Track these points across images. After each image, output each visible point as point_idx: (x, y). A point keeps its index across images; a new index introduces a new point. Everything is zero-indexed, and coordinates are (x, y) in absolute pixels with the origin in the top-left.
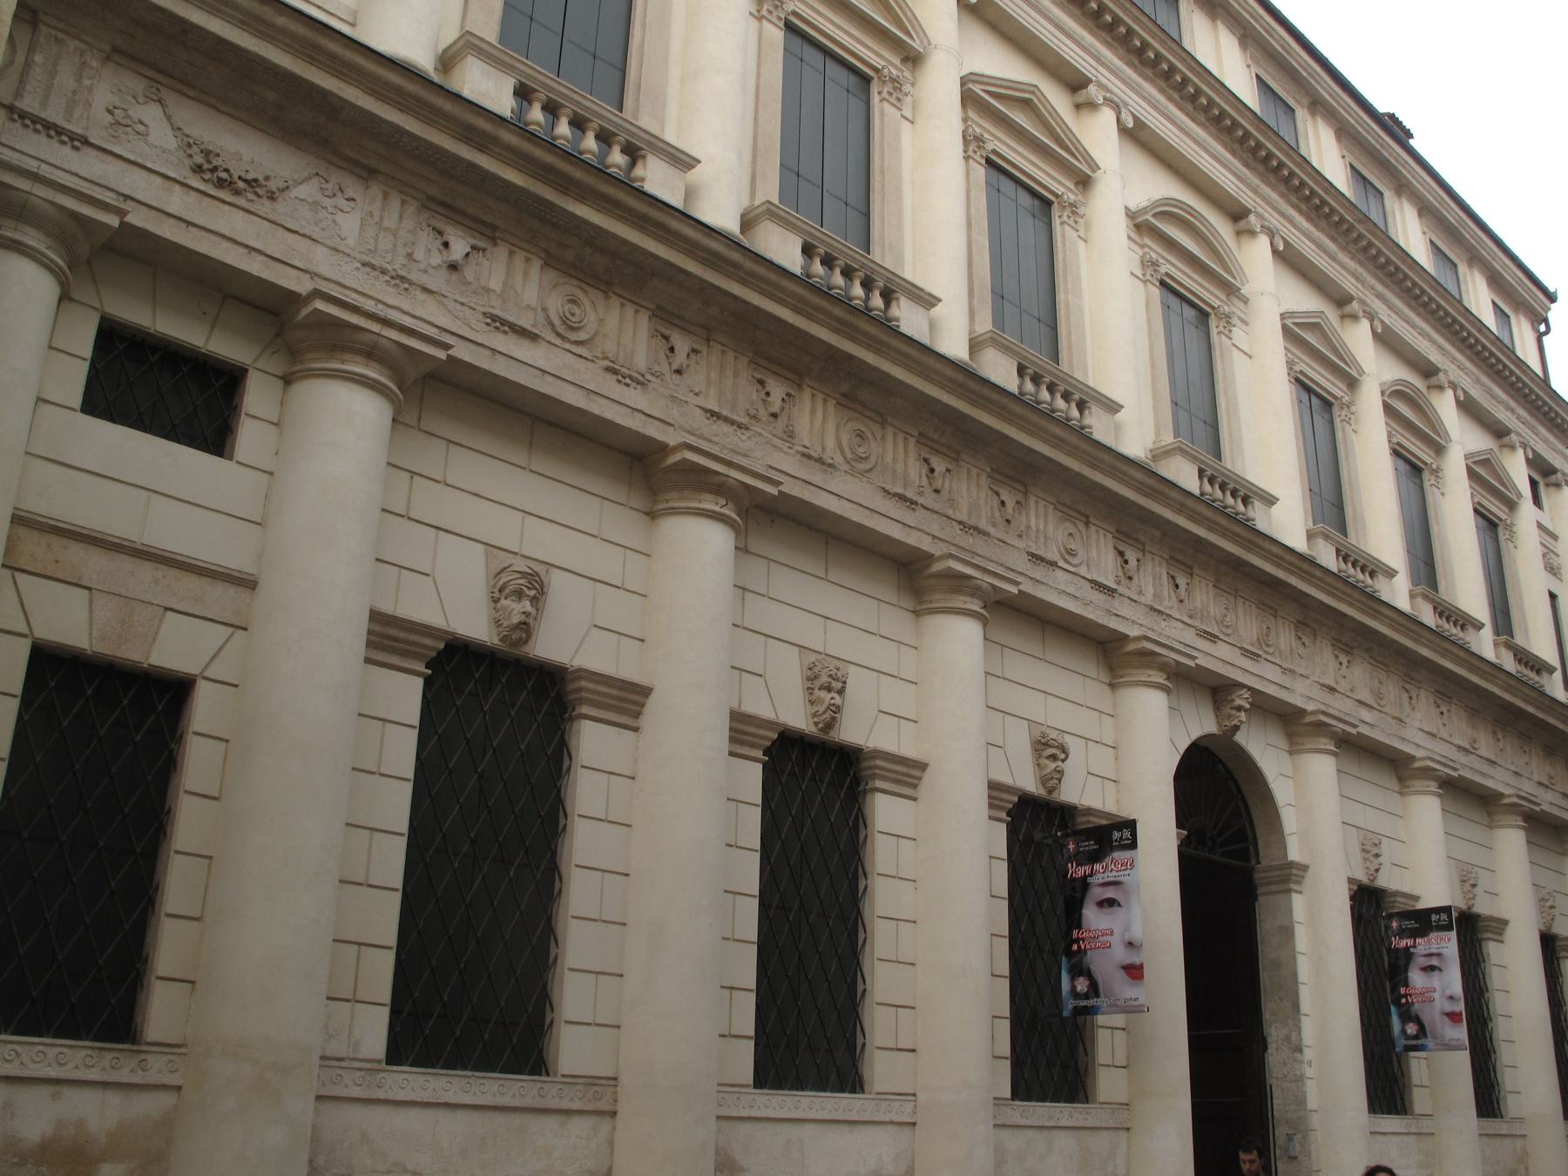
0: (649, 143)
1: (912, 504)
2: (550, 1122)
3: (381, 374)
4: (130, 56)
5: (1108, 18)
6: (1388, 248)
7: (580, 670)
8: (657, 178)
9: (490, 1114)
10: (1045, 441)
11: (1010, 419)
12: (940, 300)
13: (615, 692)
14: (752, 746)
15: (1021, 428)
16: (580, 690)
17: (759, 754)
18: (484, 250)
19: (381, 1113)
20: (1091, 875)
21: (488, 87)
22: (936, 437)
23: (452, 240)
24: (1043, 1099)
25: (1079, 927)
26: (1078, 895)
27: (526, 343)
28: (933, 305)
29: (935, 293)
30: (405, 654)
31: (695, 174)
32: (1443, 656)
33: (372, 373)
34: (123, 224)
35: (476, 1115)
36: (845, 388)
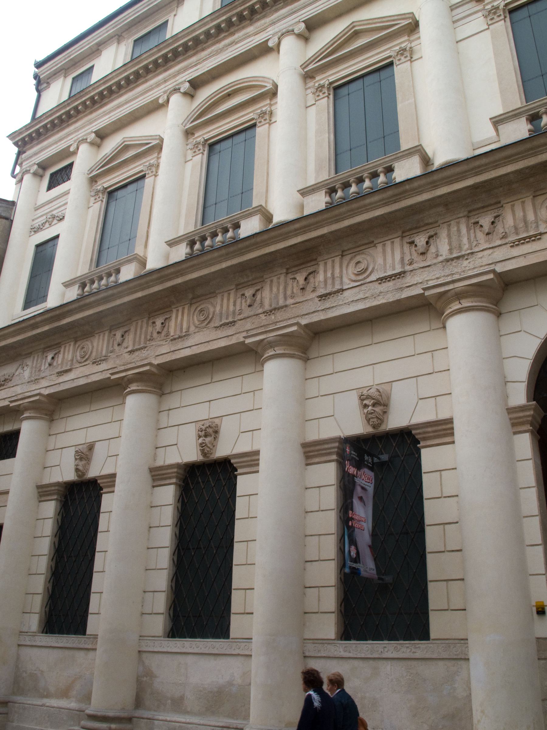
1: (233, 323)
2: (82, 653)
3: (480, 302)
4: (49, 347)
5: (234, 19)
6: (81, 97)
9: (64, 650)
10: (296, 235)
11: (266, 244)
13: (109, 480)
14: (170, 478)
15: (361, 213)
17: (334, 457)
18: (436, 234)
19: (36, 650)
22: (246, 280)
23: (28, 363)
24: (68, 633)
27: (69, 373)
32: (242, 254)
33: (466, 303)
35: (60, 650)
36: (190, 296)
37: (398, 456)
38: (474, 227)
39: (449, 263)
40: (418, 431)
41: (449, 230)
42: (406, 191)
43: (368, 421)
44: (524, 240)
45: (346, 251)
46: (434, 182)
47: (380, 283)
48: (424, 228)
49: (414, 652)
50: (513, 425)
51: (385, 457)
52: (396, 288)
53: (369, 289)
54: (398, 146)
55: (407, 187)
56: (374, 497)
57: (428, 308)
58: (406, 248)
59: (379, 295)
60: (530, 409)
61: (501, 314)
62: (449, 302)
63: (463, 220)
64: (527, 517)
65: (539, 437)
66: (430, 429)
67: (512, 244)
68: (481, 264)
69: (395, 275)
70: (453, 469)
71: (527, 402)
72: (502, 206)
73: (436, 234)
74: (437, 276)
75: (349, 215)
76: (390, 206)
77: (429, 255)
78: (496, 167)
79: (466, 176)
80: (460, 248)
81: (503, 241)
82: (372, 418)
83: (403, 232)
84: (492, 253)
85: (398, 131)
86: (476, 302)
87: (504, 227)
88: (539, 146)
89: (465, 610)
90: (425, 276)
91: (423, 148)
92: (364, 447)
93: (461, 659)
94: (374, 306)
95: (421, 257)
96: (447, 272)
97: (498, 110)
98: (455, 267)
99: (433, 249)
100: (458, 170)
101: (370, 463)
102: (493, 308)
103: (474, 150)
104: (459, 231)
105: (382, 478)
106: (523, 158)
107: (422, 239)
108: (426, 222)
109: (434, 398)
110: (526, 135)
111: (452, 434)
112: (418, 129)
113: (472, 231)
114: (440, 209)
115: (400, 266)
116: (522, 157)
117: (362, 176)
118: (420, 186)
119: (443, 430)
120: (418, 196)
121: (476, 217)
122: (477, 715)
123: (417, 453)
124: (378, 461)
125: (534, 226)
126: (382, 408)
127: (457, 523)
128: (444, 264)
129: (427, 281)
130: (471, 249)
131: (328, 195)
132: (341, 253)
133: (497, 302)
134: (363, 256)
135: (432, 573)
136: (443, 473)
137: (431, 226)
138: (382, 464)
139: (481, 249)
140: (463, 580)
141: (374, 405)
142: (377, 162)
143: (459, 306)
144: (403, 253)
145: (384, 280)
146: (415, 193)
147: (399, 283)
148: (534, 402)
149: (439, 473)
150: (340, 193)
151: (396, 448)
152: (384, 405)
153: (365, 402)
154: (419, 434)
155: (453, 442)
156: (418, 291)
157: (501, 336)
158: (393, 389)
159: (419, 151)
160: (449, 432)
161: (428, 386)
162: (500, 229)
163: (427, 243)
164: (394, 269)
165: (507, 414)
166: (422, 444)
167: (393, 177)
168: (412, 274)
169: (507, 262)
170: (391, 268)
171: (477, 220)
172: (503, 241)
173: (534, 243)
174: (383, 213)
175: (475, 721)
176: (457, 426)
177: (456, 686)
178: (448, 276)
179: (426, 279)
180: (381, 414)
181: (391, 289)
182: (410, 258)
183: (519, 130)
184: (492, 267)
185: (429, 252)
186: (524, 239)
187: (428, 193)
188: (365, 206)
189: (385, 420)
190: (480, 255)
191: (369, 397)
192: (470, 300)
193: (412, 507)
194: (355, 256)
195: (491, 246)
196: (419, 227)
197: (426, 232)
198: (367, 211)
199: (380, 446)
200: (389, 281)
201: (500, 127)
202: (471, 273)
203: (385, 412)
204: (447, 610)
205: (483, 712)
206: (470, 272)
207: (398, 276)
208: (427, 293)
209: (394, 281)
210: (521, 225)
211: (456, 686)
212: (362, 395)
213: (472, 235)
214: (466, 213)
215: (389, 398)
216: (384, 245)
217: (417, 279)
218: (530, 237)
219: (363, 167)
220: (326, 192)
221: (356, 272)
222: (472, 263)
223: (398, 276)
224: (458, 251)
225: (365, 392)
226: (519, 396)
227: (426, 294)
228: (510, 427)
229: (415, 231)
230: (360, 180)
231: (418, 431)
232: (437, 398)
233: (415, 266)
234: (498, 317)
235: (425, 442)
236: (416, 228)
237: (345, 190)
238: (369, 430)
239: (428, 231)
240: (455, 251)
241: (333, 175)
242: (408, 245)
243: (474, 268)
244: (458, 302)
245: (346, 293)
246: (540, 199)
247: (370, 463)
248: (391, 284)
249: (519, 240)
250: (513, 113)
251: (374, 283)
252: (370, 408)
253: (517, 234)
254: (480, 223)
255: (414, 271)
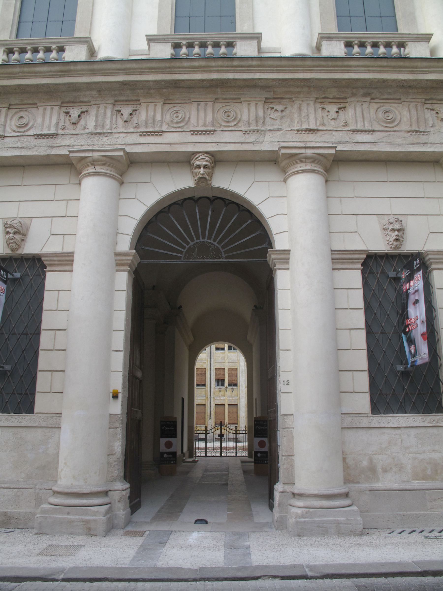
0: (236, 38)
7: (427, 251)
8: (415, 50)
12: (432, 34)
14: (357, 263)
15: (31, 77)
16: (429, 259)
17: (359, 266)
18: (87, 111)
20: (409, 289)
21: (336, 49)
25: (408, 318)
26: (405, 302)
28: (429, 39)
29: (428, 32)
30: (353, 263)
31: (433, 40)
33: (99, 169)
34: (336, 151)
37: (29, 276)
38: (117, 114)
39: (92, 136)
40: (46, 259)
41: (98, 111)
42: (70, 71)
43: (8, 244)
44: (150, 133)
45: (13, 105)
46: (94, 70)
47: (36, 138)
48: (79, 104)
49: (21, 422)
50: (117, 265)
51: (17, 275)
52: (48, 145)
53: (26, 141)
54: (73, 33)
55: (72, 68)
56: (5, 304)
57: (70, 166)
58: (62, 116)
59: (33, 148)
60: (130, 255)
61: (123, 183)
62: (87, 166)
63: (110, 106)
64: (116, 331)
65: (134, 276)
66: (55, 259)
67: (141, 134)
68: (116, 143)
69: (49, 135)
70: (68, 290)
71: (130, 250)
72: (140, 104)
73: (87, 111)
74: (82, 144)
75: (20, 76)
76: (56, 79)
77: (79, 126)
78: (142, 73)
79: (118, 73)
80: (103, 127)
81: (135, 130)
82: (12, 243)
83: (62, 103)
84: (125, 137)
85: (75, 20)
86: (107, 170)
87: (138, 120)
88: (175, 68)
89: (62, 393)
90: (73, 141)
91: (91, 40)
92: (2, 265)
93: (55, 427)
94: (28, 156)
95: (73, 126)
96: (90, 142)
97: (154, 31)
98: (97, 140)
99: (82, 122)
100: (113, 66)
101: (4, 277)
102: (118, 177)
103: (130, 55)
104: (105, 113)
105: (13, 290)
106: (163, 73)
107: (76, 112)
108: (82, 100)
109: (63, 236)
110: (169, 57)
111: (72, 265)
112: (91, 25)
113: (115, 116)
114: (94, 93)
115: (55, 129)
116: (162, 72)
117: (38, 47)
118: (83, 70)
119: (65, 260)
120: (79, 77)
121: (120, 106)
122: (61, 465)
123: (43, 275)
124: (12, 277)
125: (159, 124)
126: (21, 236)
127: (65, 330)
128: (89, 136)
129: (74, 145)
130: (111, 130)
131: (5, 54)
132: (8, 106)
133: (122, 174)
134: (26, 113)
135: (42, 364)
136: (60, 292)
137: (85, 104)
138: (15, 280)
139: (119, 132)
140: (64, 371)
141: (15, 233)
142: (53, 40)
143: (94, 170)
144: (59, 119)
145: (40, 137)
146: (77, 74)
147: (51, 142)
148: (135, 251)
149: (57, 292)
150: (16, 56)
151: (28, 269)
152: (23, 235)
153: (8, 230)
154: (47, 261)
155: (71, 271)
156: (64, 151)
157: (120, 199)
158: (32, 224)
159: (87, 41)
160: (69, 262)
161: (61, 226)
162: (135, 120)
163: (79, 116)
164: (49, 130)
165: (114, 256)
166: (48, 268)
167: (63, 56)
168: (63, 137)
169: (135, 146)
170: (47, 129)
171: (120, 109)
172: (135, 130)
173: (157, 137)
174: (48, 82)
175: (59, 470)
176: (77, 259)
177: (49, 446)
178: (90, 145)
179: (73, 144)
180: (20, 241)
181: (44, 145)
182: (63, 124)
183: (164, 51)
184: (123, 147)
185: (79, 123)
186: (150, 132)
187: (88, 78)
188: (35, 72)
189: (22, 246)
190: (117, 135)
191: (11, 226)
192: (102, 167)
193: (33, 315)
194: (20, 111)
195: (126, 131)
196: (76, 102)
197: (80, 107)
198: (36, 77)
199: (15, 266)
200: (43, 138)
201: (152, 45)
202: (107, 148)
203: (23, 240)
204: (49, 392)
205: (65, 464)
206: (107, 146)
207: (51, 137)
208: (71, 155)
209: (48, 140)
210: (151, 121)
211: (49, 446)
212: (6, 224)
213: (114, 119)
214: (113, 101)
215: (28, 230)
216: (45, 109)
217: (66, 142)
218: (155, 132)
219: (40, 40)
220: (4, 51)
221: (18, 125)
222: (109, 140)
223: (51, 137)
224: (101, 129)
225: (9, 222)
226: (125, 244)
227: (70, 155)
228: (114, 265)
229: (71, 105)
230: (36, 50)
231: (46, 259)
232: (65, 236)
233: (66, 132)
234: (121, 185)
235: (50, 267)
236: (73, 102)
237: (22, 54)
238: (8, 252)
239: (82, 107)
240: (99, 128)
241: (13, 38)
242: (64, 114)
243: (110, 145)
244: (93, 167)
245: (7, 140)
246: (167, 107)
247: (4, 277)
248: (45, 141)
249: (147, 132)
250: (163, 37)
251: (31, 137)
252: (11, 235)
253: (146, 127)
254: (122, 112)
255: (65, 136)
